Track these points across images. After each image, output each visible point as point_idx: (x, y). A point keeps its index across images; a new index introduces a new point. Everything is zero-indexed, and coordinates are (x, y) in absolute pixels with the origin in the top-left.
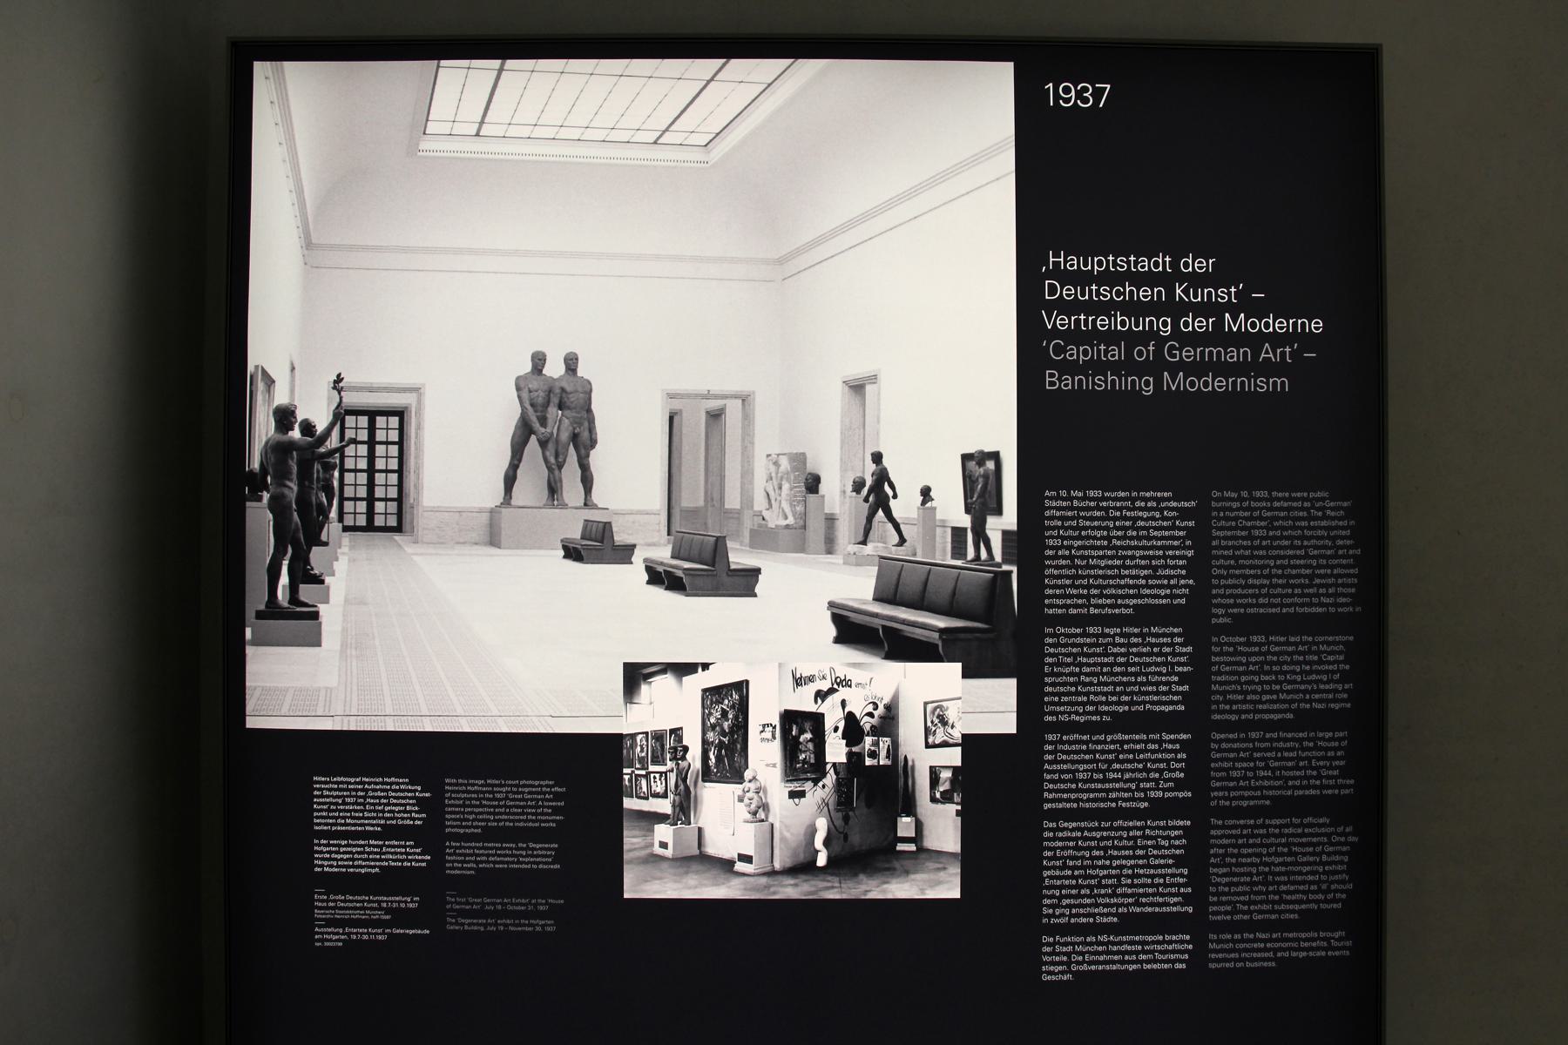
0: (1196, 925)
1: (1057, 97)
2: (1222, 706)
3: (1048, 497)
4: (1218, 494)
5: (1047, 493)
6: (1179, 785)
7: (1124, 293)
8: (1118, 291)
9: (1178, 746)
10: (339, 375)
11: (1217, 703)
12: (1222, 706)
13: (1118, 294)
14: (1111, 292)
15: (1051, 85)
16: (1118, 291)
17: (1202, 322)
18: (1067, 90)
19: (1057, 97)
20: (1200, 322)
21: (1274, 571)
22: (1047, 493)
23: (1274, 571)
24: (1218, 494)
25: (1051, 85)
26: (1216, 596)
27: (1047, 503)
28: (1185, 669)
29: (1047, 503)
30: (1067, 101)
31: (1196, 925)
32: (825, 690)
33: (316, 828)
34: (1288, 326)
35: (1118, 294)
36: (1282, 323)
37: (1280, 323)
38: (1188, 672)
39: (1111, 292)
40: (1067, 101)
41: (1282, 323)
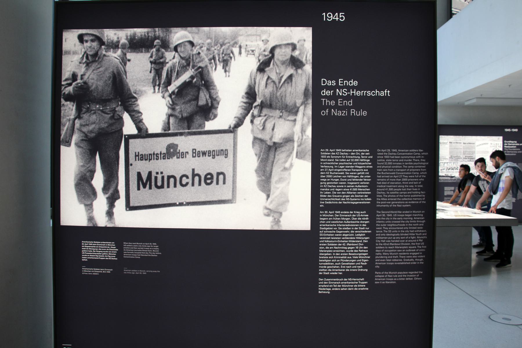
0: (369, 276)
1: (326, 17)
2: (380, 244)
3: (322, 151)
4: (380, 150)
5: (321, 150)
6: (364, 267)
7: (375, 93)
8: (373, 93)
9: (366, 225)
10: (510, 87)
11: (378, 243)
12: (380, 244)
13: (373, 93)
14: (371, 93)
15: (324, 14)
16: (373, 93)
17: (359, 92)
18: (330, 15)
19: (326, 17)
20: (328, 92)
21: (409, 225)
22: (321, 150)
23: (409, 225)
24: (380, 150)
25: (324, 14)
26: (378, 236)
27: (322, 153)
28: (370, 167)
29: (322, 153)
30: (330, 19)
31: (369, 276)
32: (440, 32)
33: (83, 260)
34: (361, 94)
35: (373, 93)
36: (328, 92)
37: (328, 92)
38: (369, 204)
39: (371, 93)
40: (330, 19)
41: (328, 92)
